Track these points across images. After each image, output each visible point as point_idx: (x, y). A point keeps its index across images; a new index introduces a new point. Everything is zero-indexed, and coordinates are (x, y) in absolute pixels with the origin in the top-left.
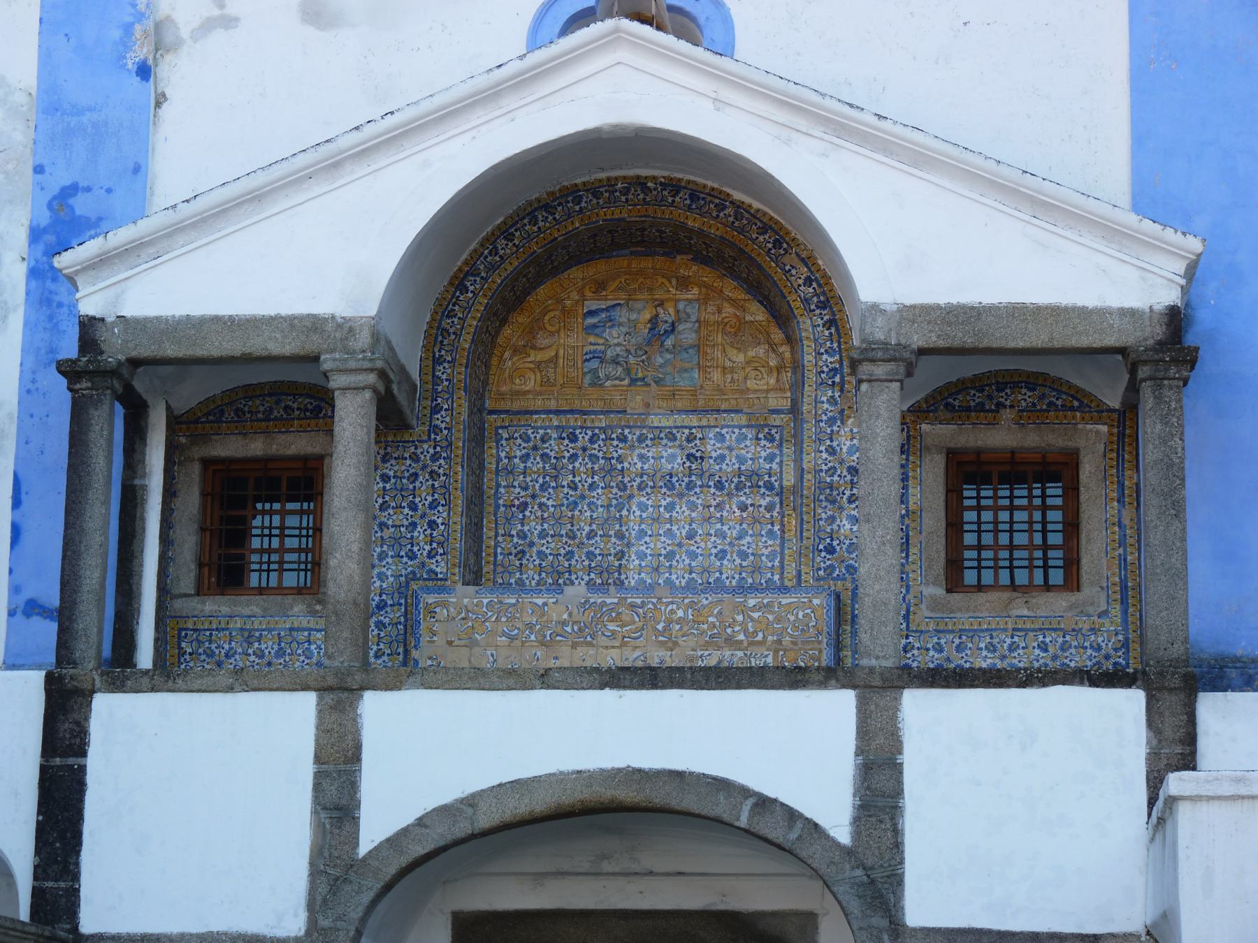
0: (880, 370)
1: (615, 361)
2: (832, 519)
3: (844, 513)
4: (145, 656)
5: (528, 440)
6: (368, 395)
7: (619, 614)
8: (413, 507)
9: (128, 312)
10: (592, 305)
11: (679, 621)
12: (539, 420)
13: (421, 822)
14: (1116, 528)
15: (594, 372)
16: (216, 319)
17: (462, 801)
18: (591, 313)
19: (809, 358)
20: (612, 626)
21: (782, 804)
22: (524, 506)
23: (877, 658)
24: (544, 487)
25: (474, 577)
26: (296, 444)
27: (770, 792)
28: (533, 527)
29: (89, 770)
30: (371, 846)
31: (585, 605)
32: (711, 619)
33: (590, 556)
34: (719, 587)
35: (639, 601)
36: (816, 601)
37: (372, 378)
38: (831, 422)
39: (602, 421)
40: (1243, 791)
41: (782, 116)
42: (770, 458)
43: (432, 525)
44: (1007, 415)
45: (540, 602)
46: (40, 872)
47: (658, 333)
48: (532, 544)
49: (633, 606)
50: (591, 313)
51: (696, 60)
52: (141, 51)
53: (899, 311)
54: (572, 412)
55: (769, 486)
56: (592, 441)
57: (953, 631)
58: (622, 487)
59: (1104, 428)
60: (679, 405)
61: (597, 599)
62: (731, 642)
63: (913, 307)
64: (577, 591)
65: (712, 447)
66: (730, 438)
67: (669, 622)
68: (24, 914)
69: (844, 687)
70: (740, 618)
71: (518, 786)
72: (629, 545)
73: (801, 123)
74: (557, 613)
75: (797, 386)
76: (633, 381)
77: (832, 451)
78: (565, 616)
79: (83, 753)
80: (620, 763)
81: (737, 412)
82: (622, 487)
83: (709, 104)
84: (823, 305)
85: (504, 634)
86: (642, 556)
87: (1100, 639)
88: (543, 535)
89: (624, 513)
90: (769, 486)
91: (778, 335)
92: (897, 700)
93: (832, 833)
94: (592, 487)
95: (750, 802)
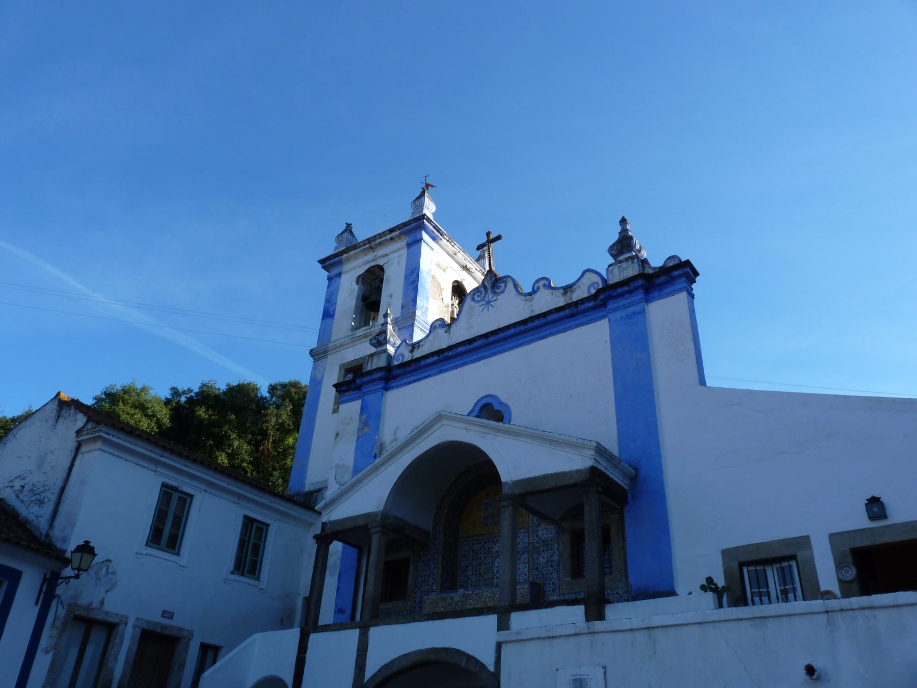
0: (505, 503)
2: (537, 558)
3: (541, 556)
5: (468, 545)
7: (472, 597)
9: (331, 520)
11: (489, 597)
13: (380, 670)
14: (622, 550)
16: (349, 518)
17: (390, 662)
20: (471, 601)
21: (475, 658)
22: (467, 566)
23: (504, 602)
24: (473, 560)
27: (471, 653)
28: (470, 573)
29: (307, 658)
30: (369, 677)
31: (464, 595)
32: (497, 596)
33: (485, 580)
35: (477, 592)
36: (526, 586)
37: (379, 529)
38: (537, 526)
40: (520, 638)
41: (482, 430)
49: (476, 594)
51: (475, 422)
52: (376, 451)
53: (512, 483)
57: (572, 593)
59: (617, 516)
61: (467, 593)
63: (516, 481)
67: (486, 598)
69: (493, 614)
71: (405, 656)
72: (494, 575)
73: (487, 431)
77: (537, 536)
78: (458, 599)
80: (431, 646)
81: (523, 528)
83: (465, 431)
85: (442, 607)
87: (619, 591)
88: (472, 575)
89: (493, 565)
92: (510, 614)
93: (489, 668)
94: (485, 558)
95: (465, 658)
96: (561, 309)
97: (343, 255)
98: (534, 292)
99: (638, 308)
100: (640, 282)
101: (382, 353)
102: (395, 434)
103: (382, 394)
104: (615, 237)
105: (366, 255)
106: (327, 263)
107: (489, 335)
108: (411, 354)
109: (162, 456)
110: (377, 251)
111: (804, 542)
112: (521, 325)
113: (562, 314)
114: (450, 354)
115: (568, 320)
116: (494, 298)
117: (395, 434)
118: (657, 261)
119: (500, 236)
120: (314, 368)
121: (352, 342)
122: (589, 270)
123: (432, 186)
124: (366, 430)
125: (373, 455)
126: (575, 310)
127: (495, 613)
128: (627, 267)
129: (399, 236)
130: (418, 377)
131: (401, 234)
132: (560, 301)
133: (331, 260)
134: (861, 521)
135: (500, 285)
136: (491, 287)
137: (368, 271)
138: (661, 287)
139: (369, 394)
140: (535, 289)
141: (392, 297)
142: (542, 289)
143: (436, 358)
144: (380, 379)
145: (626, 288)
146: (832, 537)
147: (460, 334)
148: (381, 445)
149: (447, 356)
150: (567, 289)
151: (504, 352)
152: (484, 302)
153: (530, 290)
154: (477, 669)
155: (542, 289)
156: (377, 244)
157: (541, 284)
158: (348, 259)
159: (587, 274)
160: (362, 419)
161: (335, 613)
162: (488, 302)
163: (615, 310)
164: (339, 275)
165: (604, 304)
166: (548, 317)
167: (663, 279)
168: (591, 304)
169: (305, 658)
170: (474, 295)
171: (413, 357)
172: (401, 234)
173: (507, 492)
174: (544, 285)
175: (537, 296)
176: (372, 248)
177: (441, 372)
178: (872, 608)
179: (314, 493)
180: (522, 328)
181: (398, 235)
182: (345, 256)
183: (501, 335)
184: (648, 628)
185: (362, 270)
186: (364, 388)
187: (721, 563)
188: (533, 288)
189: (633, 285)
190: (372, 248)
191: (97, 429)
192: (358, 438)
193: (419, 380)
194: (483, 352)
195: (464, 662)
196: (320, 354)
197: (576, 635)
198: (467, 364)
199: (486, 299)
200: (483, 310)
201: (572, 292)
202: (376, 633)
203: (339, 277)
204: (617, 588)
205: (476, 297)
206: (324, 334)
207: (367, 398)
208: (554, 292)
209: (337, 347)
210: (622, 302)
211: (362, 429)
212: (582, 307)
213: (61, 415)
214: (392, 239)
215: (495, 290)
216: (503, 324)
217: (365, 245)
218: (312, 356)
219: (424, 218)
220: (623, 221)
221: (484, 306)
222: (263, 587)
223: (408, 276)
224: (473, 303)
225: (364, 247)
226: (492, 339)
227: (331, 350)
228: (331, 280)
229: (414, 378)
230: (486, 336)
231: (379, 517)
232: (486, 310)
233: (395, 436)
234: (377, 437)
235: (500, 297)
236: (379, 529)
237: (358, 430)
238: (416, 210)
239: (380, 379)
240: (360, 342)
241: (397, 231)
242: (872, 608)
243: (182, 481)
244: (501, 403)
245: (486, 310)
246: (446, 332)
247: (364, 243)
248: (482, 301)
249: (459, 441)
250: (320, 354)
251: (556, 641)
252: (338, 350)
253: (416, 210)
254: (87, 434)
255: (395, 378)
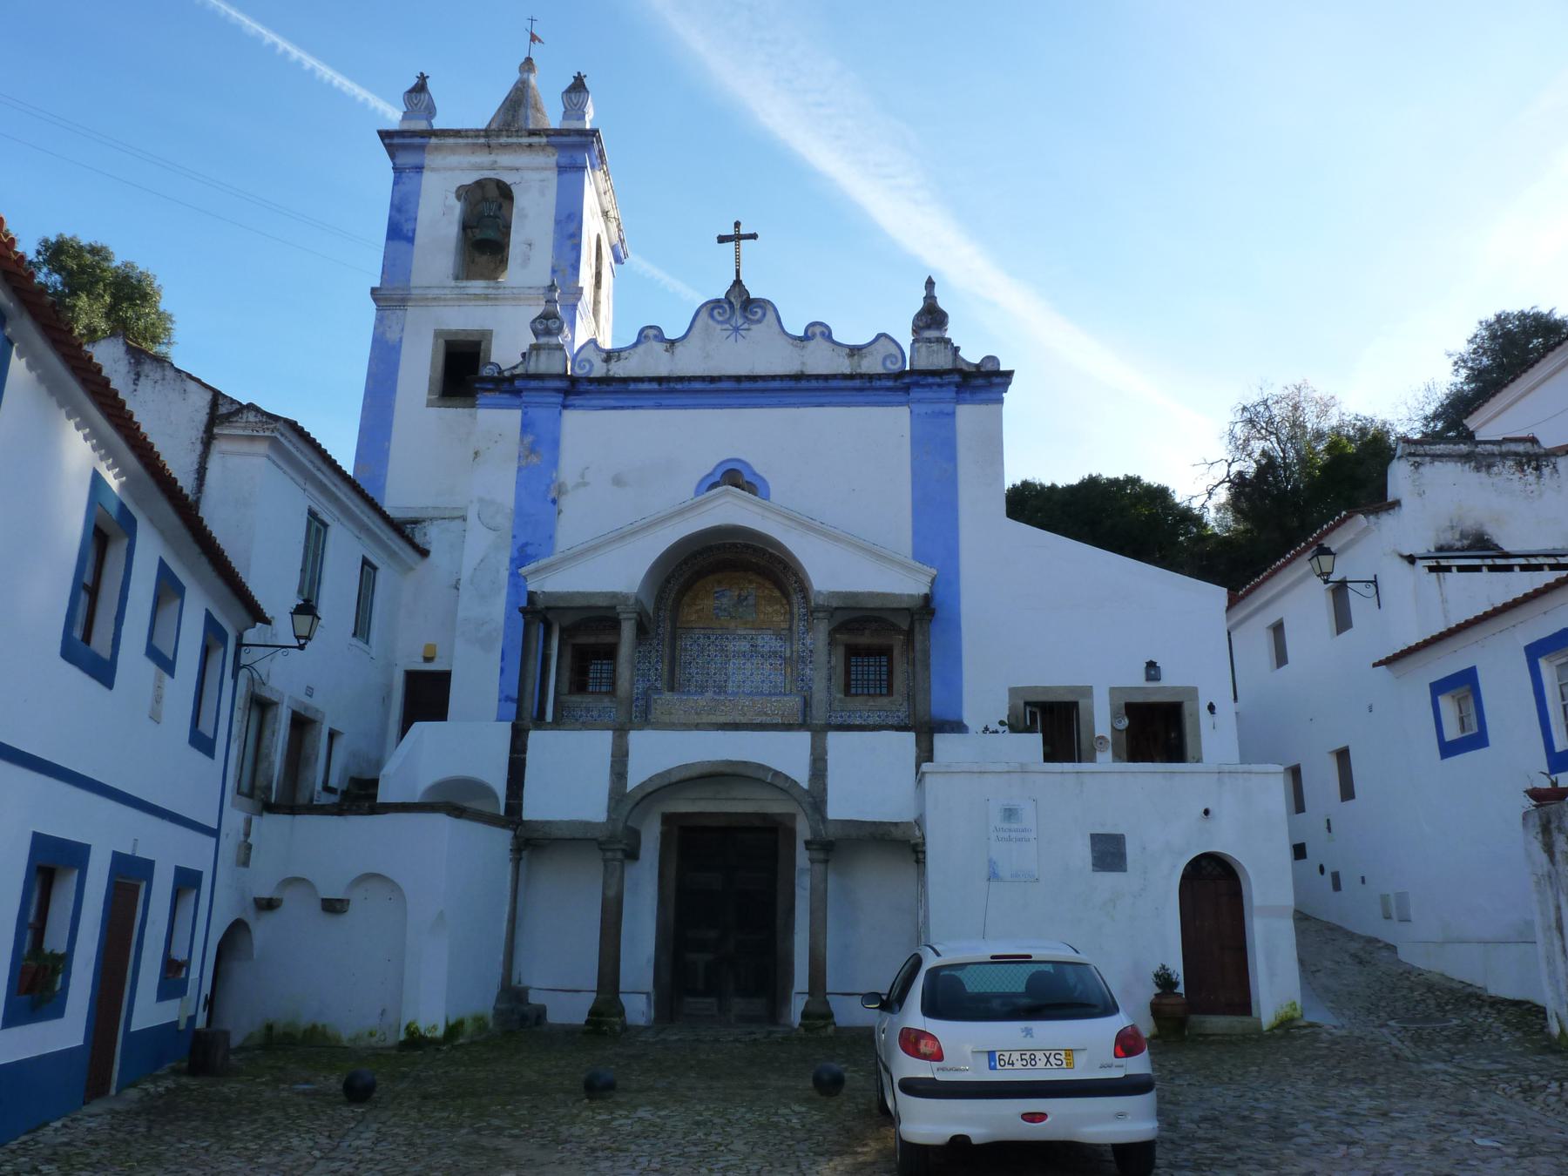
0: (821, 615)
1: (725, 610)
2: (803, 669)
4: (549, 717)
6: (633, 621)
8: (650, 663)
10: (717, 589)
12: (697, 631)
13: (650, 779)
15: (717, 613)
18: (716, 592)
19: (795, 610)
20: (722, 708)
22: (690, 663)
25: (672, 689)
26: (607, 639)
27: (779, 769)
34: (762, 694)
37: (635, 615)
38: (803, 634)
39: (720, 632)
41: (787, 522)
42: (781, 647)
43: (657, 669)
44: (867, 632)
45: (696, 698)
46: (508, 797)
47: (741, 600)
48: (693, 677)
50: (716, 592)
52: (553, 494)
54: (709, 628)
55: (781, 657)
56: (716, 639)
58: (727, 656)
59: (901, 637)
60: (748, 626)
61: (716, 697)
62: (766, 714)
64: (709, 695)
65: (760, 642)
66: (767, 638)
67: (743, 706)
68: (502, 812)
70: (769, 705)
74: (702, 703)
75: (792, 620)
76: (731, 618)
77: (803, 644)
79: (525, 752)
81: (770, 629)
82: (727, 656)
84: (800, 591)
86: (734, 682)
88: (697, 673)
90: (781, 657)
91: (784, 602)
92: (826, 736)
93: (801, 784)
94: (716, 656)
96: (845, 377)
97: (430, 138)
98: (806, 338)
99: (947, 408)
100: (957, 378)
101: (557, 349)
102: (582, 476)
103: (560, 414)
104: (919, 305)
105: (473, 153)
106: (396, 141)
107: (743, 379)
108: (605, 364)
109: (319, 470)
110: (497, 154)
111: (1087, 691)
112: (790, 380)
113: (849, 383)
114: (679, 386)
115: (854, 393)
116: (746, 326)
117: (582, 476)
118: (972, 355)
119: (757, 236)
120: (380, 321)
121: (459, 299)
122: (884, 335)
123: (540, 41)
124: (534, 459)
125: (549, 499)
126: (868, 384)
127: (807, 730)
128: (938, 351)
129: (543, 147)
130: (621, 404)
131: (549, 144)
132: (844, 366)
133: (404, 137)
134: (1137, 679)
135: (755, 310)
136: (741, 307)
137: (480, 184)
138: (975, 389)
139: (536, 407)
140: (809, 334)
141: (532, 247)
142: (819, 338)
143: (655, 386)
144: (558, 390)
145: (938, 380)
146: (1112, 690)
147: (688, 363)
148: (560, 486)
149: (674, 388)
150: (855, 351)
151: (762, 407)
152: (728, 326)
153: (801, 333)
154: (787, 785)
155: (819, 338)
156: (501, 145)
157: (818, 330)
158: (437, 148)
159: (883, 338)
160: (525, 442)
161: (500, 700)
162: (737, 329)
163: (919, 401)
164: (419, 169)
165: (907, 389)
166: (830, 381)
167: (980, 382)
168: (890, 383)
169: (524, 759)
170: (713, 309)
171: (608, 370)
172: (549, 144)
173: (821, 603)
174: (823, 334)
175: (812, 344)
176: (489, 147)
177: (659, 406)
178: (1250, 773)
179: (408, 523)
180: (792, 384)
181: (543, 144)
182: (433, 141)
183: (760, 385)
184: (1078, 772)
185: (469, 178)
186: (526, 396)
187: (1007, 700)
188: (806, 331)
189: (947, 379)
190: (489, 147)
191: (272, 426)
192: (520, 469)
193: (622, 408)
194: (728, 398)
195: (770, 777)
196: (392, 300)
197: (1008, 772)
198: (704, 408)
199: (733, 322)
200: (727, 338)
201: (862, 357)
202: (639, 740)
203: (418, 172)
204: (898, 711)
205: (716, 312)
206: (395, 266)
207: (531, 411)
208: (838, 349)
209: (427, 299)
210: (928, 394)
211: (527, 457)
212: (877, 384)
213: (142, 374)
214: (530, 145)
215: (747, 314)
216: (761, 370)
217: (477, 136)
218: (375, 300)
219: (594, 135)
220: (930, 284)
221: (729, 332)
222: (373, 655)
223: (561, 221)
224: (711, 322)
225: (475, 141)
226: (745, 385)
227: (416, 300)
228: (400, 172)
229: (613, 403)
230: (738, 379)
231: (632, 601)
232: (732, 338)
233: (583, 478)
234: (554, 475)
235: (754, 327)
236: (635, 615)
237: (520, 457)
238: (569, 107)
239: (558, 390)
240: (473, 303)
241: (542, 137)
242: (1250, 773)
243: (327, 508)
244: (755, 474)
245: (732, 338)
246: (667, 350)
247: (477, 133)
248: (727, 323)
249: (757, 531)
250: (392, 300)
251: (986, 775)
252: (429, 304)
253: (569, 107)
254: (245, 428)
255: (579, 393)
